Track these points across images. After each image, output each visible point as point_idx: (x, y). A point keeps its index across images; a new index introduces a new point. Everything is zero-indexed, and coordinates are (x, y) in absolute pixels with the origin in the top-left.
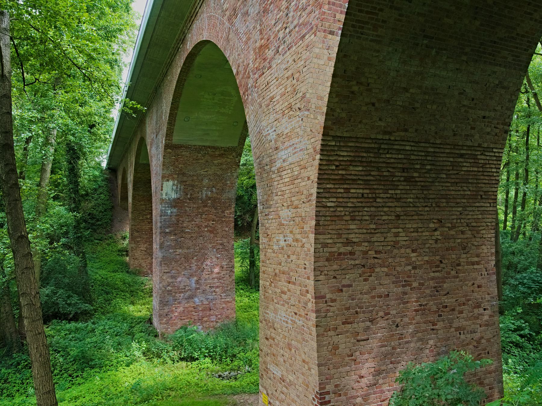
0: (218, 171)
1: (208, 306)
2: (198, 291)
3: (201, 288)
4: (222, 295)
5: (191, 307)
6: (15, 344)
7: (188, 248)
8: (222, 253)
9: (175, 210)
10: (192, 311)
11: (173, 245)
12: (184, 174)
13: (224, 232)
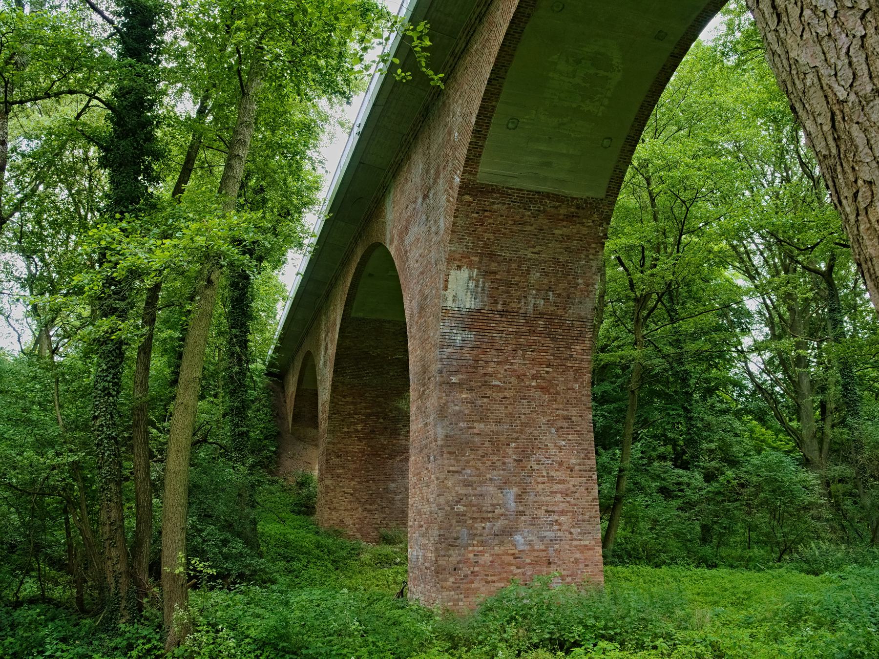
0: (561, 253)
1: (544, 554)
2: (523, 518)
3: (527, 513)
4: (572, 530)
5: (508, 555)
6: (124, 604)
7: (498, 422)
8: (570, 437)
9: (470, 336)
10: (510, 564)
11: (467, 412)
12: (492, 256)
13: (570, 391)
